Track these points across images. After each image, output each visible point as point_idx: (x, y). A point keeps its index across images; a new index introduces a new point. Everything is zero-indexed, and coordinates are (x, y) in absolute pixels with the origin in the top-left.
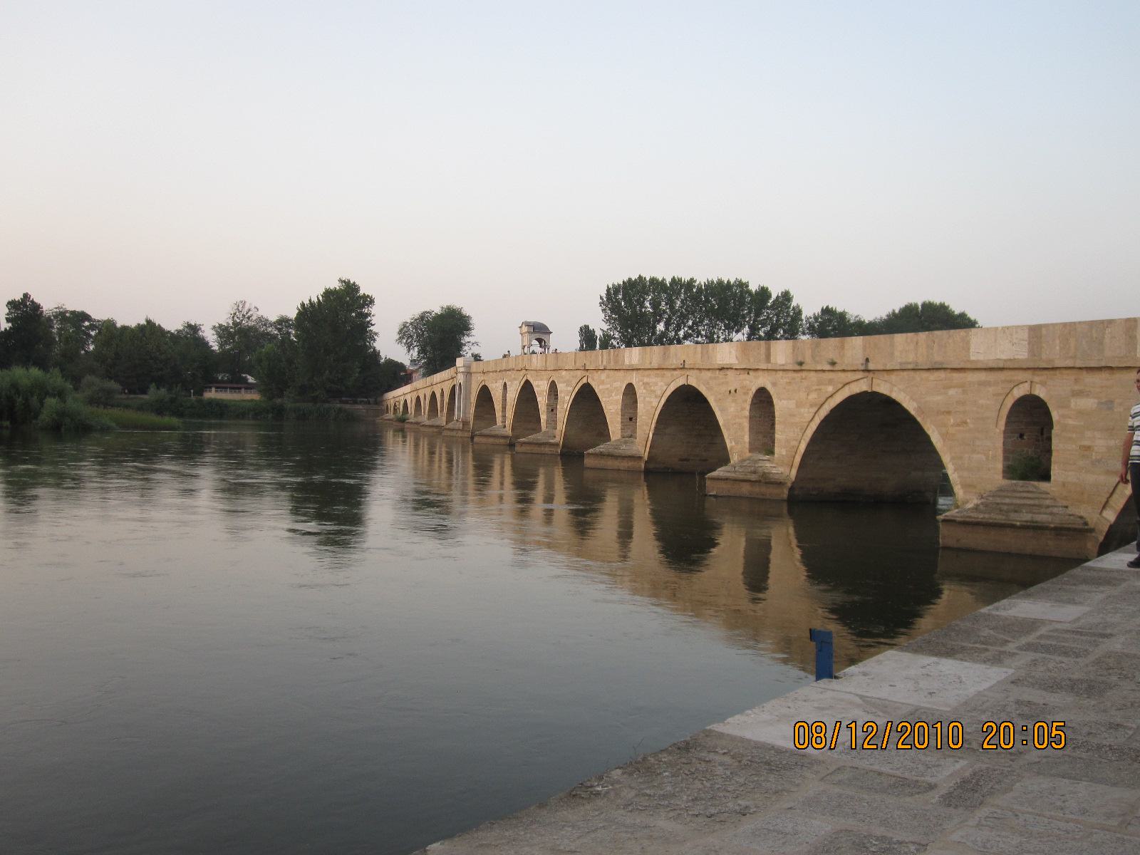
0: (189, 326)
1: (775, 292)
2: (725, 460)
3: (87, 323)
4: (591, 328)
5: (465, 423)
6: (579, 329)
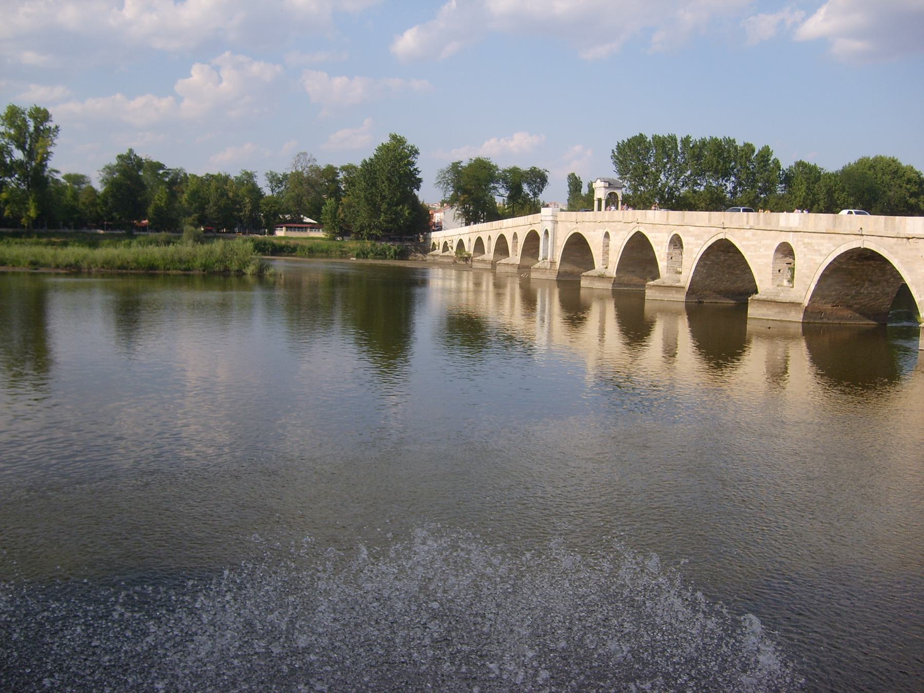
0: (247, 173)
1: (758, 148)
2: (756, 292)
3: (161, 172)
4: (577, 175)
5: (553, 263)
6: (567, 177)
